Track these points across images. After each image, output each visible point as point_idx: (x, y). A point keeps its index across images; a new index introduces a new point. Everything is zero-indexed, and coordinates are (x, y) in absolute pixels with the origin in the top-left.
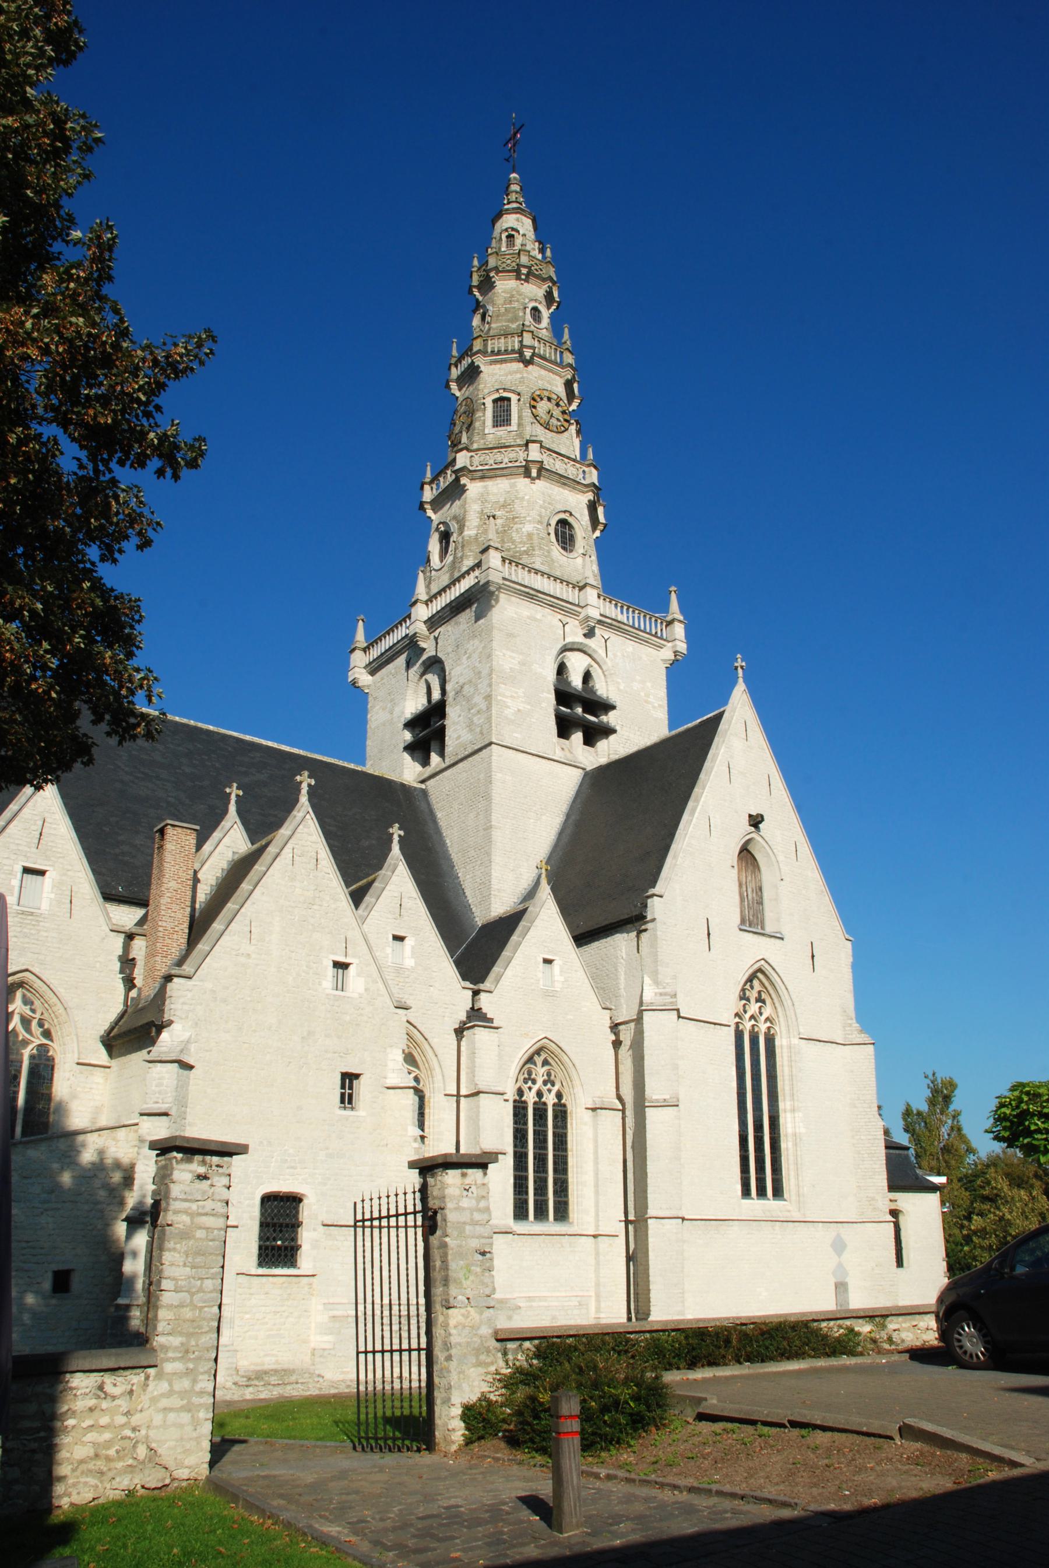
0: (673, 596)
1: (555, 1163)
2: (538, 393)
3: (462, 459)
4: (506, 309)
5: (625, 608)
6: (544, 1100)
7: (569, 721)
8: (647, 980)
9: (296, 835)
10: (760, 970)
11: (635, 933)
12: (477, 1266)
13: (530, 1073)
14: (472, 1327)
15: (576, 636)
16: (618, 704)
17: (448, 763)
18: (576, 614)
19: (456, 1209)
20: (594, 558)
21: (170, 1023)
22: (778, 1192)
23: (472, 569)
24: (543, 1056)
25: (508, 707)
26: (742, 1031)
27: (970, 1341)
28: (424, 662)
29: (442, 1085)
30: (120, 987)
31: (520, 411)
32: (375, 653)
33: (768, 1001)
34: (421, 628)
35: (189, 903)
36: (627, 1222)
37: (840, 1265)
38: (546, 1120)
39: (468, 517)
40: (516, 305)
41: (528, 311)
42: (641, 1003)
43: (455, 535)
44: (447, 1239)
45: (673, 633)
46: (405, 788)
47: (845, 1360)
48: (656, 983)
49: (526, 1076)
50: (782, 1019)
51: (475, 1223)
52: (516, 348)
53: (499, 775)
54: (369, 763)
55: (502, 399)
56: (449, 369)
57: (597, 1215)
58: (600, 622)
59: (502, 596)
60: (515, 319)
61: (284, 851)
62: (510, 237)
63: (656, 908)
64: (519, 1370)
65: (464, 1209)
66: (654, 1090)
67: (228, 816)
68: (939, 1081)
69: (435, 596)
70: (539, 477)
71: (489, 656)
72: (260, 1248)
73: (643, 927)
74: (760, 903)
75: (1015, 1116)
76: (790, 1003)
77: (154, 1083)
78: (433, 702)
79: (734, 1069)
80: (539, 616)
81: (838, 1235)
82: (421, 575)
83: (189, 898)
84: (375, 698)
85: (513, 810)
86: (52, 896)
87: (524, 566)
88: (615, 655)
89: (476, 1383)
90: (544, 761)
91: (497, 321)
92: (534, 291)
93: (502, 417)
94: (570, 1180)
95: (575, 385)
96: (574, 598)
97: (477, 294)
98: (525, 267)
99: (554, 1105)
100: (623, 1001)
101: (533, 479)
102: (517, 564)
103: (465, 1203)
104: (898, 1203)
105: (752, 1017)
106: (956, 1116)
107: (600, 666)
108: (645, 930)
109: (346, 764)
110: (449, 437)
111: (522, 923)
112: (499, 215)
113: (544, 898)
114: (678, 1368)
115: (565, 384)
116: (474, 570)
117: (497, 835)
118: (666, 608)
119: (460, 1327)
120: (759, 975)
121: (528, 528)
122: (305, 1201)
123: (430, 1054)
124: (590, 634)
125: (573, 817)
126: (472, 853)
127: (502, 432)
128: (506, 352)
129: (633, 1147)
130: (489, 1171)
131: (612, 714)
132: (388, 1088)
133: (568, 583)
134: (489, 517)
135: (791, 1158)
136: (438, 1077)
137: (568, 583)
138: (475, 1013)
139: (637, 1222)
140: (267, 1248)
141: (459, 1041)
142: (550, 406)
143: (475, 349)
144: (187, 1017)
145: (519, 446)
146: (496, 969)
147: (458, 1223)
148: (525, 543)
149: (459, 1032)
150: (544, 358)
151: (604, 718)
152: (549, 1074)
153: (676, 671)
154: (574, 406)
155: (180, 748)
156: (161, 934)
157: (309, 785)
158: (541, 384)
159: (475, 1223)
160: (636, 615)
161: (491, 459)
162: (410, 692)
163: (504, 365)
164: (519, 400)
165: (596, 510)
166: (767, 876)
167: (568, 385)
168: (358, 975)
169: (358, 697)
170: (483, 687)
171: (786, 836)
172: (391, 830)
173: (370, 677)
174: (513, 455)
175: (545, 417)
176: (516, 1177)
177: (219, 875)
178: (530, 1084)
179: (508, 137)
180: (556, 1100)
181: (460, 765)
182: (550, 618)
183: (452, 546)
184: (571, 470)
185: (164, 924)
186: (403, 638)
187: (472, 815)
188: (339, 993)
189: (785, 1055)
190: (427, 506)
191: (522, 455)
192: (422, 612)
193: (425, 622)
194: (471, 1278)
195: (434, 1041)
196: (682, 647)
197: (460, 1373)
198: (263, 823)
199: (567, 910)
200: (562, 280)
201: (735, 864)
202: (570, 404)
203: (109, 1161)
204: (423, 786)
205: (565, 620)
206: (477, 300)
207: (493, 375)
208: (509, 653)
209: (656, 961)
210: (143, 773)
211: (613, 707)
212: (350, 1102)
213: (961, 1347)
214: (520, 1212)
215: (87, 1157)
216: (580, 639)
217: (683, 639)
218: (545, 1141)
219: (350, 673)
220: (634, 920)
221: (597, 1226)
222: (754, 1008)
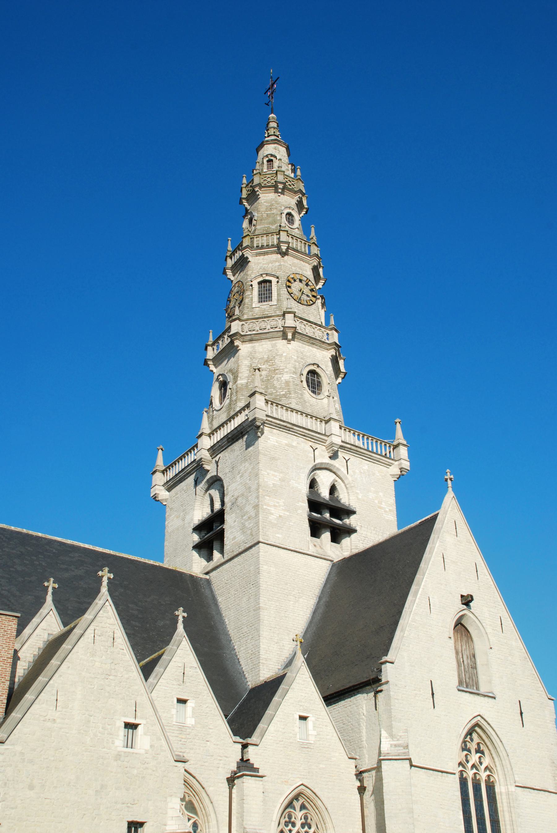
3: (235, 327)
4: (267, 215)
5: (361, 436)
7: (320, 524)
8: (384, 733)
9: (97, 619)
10: (477, 725)
11: (373, 694)
13: (290, 817)
15: (323, 457)
16: (357, 510)
17: (227, 557)
18: (324, 441)
23: (243, 409)
24: (301, 801)
26: (466, 779)
28: (208, 480)
29: (216, 829)
31: (278, 290)
32: (171, 474)
33: (486, 752)
34: (205, 454)
35: (8, 678)
39: (241, 370)
40: (274, 211)
42: (380, 753)
43: (231, 384)
45: (398, 454)
48: (391, 736)
50: (499, 768)
52: (275, 243)
53: (265, 567)
54: (166, 560)
55: (265, 281)
56: (226, 260)
58: (341, 447)
59: (266, 428)
60: (274, 222)
61: (87, 632)
62: (270, 161)
63: (389, 672)
69: (216, 430)
70: (293, 339)
71: (257, 475)
73: (379, 689)
74: (475, 667)
76: (505, 755)
78: (215, 511)
80: (294, 444)
82: (205, 414)
83: (8, 674)
85: (277, 595)
87: (282, 406)
88: (354, 472)
92: (289, 201)
95: (321, 270)
100: (365, 751)
102: (277, 405)
105: (474, 766)
108: (381, 691)
109: (147, 561)
111: (282, 686)
112: (262, 145)
113: (299, 665)
117: (264, 615)
118: (393, 435)
120: (477, 729)
121: (286, 377)
124: (334, 456)
125: (324, 600)
126: (245, 629)
127: (265, 306)
131: (353, 517)
133: (317, 418)
134: (255, 369)
136: (213, 822)
137: (317, 418)
138: (245, 764)
141: (231, 788)
143: (244, 245)
145: (278, 316)
146: (261, 726)
148: (283, 389)
149: (231, 781)
150: (297, 251)
151: (347, 521)
152: (306, 818)
153: (401, 480)
154: (320, 285)
155: (14, 551)
158: (294, 269)
160: (370, 441)
161: (257, 326)
162: (197, 504)
163: (266, 257)
164: (278, 282)
165: (337, 362)
166: (479, 645)
167: (315, 269)
168: (145, 734)
171: (491, 612)
172: (177, 613)
173: (167, 493)
174: (273, 323)
177: (36, 653)
179: (268, 87)
181: (236, 560)
182: (305, 445)
183: (229, 392)
184: (318, 333)
186: (192, 462)
187: (245, 599)
188: (129, 750)
189: (505, 801)
190: (210, 363)
191: (280, 323)
192: (206, 443)
193: (208, 450)
195: (210, 790)
196: (406, 465)
198: (73, 610)
199: (318, 675)
200: (310, 192)
204: (207, 577)
206: (246, 208)
207: (258, 264)
208: (272, 472)
209: (390, 717)
211: (354, 512)
216: (327, 460)
219: (152, 490)
220: (372, 683)
222: (474, 758)
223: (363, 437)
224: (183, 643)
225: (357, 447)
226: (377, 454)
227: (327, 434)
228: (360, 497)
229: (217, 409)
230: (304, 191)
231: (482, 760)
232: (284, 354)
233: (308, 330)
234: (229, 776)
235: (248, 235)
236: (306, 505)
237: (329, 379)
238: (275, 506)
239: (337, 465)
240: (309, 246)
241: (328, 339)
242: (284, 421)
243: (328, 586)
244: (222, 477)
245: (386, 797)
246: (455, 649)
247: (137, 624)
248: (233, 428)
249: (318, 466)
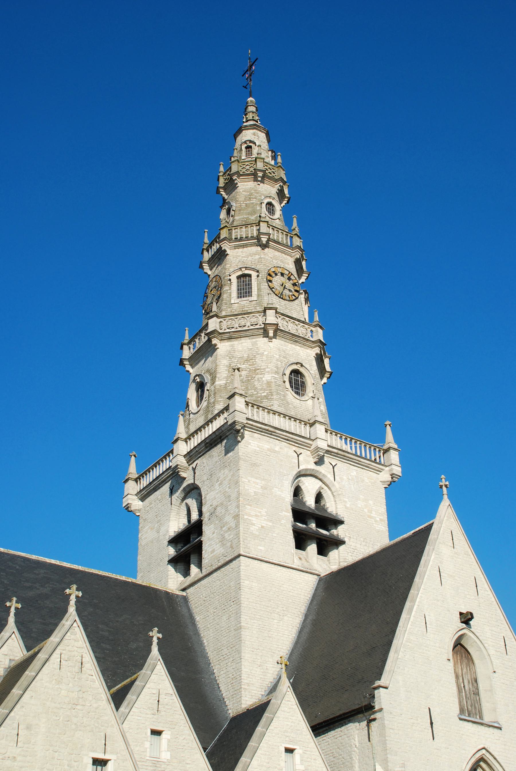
2: (273, 270)
4: (246, 205)
10: (482, 759)
11: (365, 723)
15: (308, 462)
16: (345, 519)
17: (205, 572)
18: (309, 446)
20: (322, 400)
23: (222, 412)
25: (254, 524)
31: (259, 285)
32: (145, 482)
34: (181, 461)
40: (254, 201)
41: (264, 205)
43: (208, 385)
45: (389, 459)
52: (255, 235)
53: (247, 582)
54: (139, 575)
55: (244, 276)
56: (202, 253)
58: (327, 452)
59: (246, 433)
60: (254, 212)
61: (52, 657)
62: (249, 148)
63: (382, 698)
69: (192, 435)
70: (275, 336)
71: (237, 483)
73: (372, 717)
80: (277, 449)
82: (181, 418)
84: (145, 520)
85: (259, 614)
87: (264, 408)
88: (341, 479)
92: (269, 190)
93: (245, 290)
95: (304, 263)
96: (306, 433)
97: (223, 193)
101: (271, 338)
102: (259, 407)
107: (329, 488)
108: (374, 720)
109: (118, 577)
110: (203, 307)
111: (266, 715)
112: (240, 131)
113: (285, 690)
115: (295, 262)
116: (223, 413)
117: (246, 635)
118: (383, 439)
120: (482, 764)
121: (267, 377)
124: (320, 462)
125: (310, 618)
126: (225, 651)
127: (244, 302)
131: (341, 528)
134: (235, 369)
137: (301, 421)
142: (284, 280)
143: (222, 237)
145: (258, 312)
148: (265, 390)
151: (334, 532)
153: (392, 487)
154: (303, 279)
157: (77, 597)
158: (275, 263)
160: (358, 445)
161: (236, 323)
162: (173, 514)
163: (245, 249)
164: (258, 276)
165: (322, 361)
166: (481, 669)
167: (298, 263)
170: (232, 509)
172: (151, 634)
173: (141, 503)
174: (254, 320)
175: (280, 289)
179: (245, 70)
181: (215, 574)
182: (287, 450)
184: (301, 330)
187: (225, 618)
190: (186, 362)
191: (260, 320)
192: (182, 448)
193: (185, 456)
196: (398, 470)
198: (37, 632)
199: (305, 702)
200: (291, 180)
201: (451, 657)
202: (300, 278)
204: (184, 594)
205: (299, 451)
206: (224, 198)
207: (237, 257)
208: (253, 480)
211: (342, 522)
216: (312, 466)
217: (398, 464)
219: (124, 500)
223: (351, 441)
224: (157, 667)
225: (344, 451)
226: (365, 458)
228: (348, 506)
230: (285, 180)
232: (265, 353)
235: (226, 226)
236: (290, 515)
237: (314, 379)
238: (256, 516)
239: (323, 472)
240: (291, 238)
241: (312, 336)
242: (266, 425)
244: (200, 485)
246: (455, 672)
248: (211, 433)
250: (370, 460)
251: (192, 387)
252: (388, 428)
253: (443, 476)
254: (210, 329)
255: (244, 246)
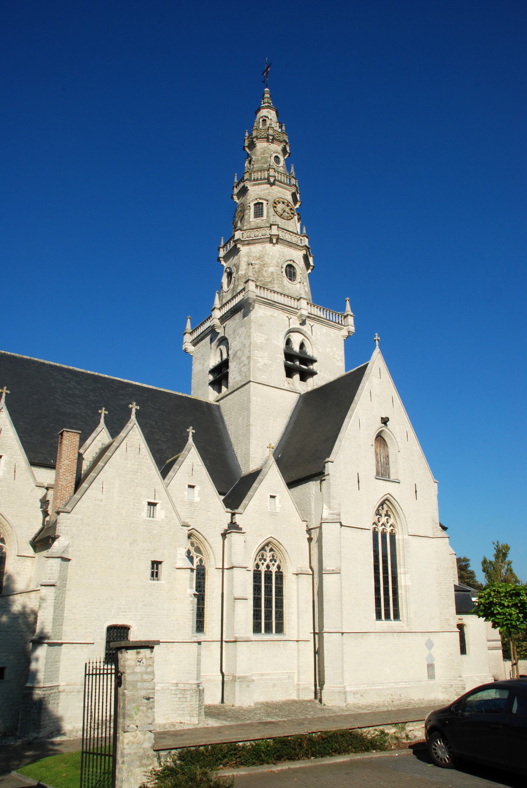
0: (348, 302)
1: (276, 603)
2: (277, 200)
5: (322, 309)
6: (270, 569)
7: (292, 369)
8: (325, 506)
9: (128, 436)
10: (387, 499)
11: (319, 481)
12: (144, 706)
13: (263, 556)
14: (139, 743)
15: (295, 323)
16: (318, 359)
18: (296, 313)
19: (132, 673)
21: (59, 536)
22: (397, 616)
23: (241, 291)
24: (270, 546)
25: (259, 362)
26: (377, 532)
27: (441, 750)
28: (219, 339)
29: (214, 563)
30: (41, 515)
31: (268, 209)
32: (196, 335)
33: (392, 516)
34: (217, 322)
36: (315, 633)
37: (430, 655)
38: (272, 580)
40: (266, 155)
41: (273, 158)
43: (234, 274)
44: (126, 691)
45: (347, 322)
46: (208, 405)
47: (375, 754)
48: (330, 508)
49: (261, 557)
50: (399, 525)
51: (143, 681)
52: (266, 177)
53: (254, 398)
55: (259, 203)
56: (233, 189)
57: (298, 630)
58: (308, 317)
59: (256, 305)
60: (266, 162)
62: (264, 121)
63: (330, 468)
64: (167, 768)
65: (137, 673)
66: (327, 565)
67: (100, 425)
68: (500, 546)
70: (277, 243)
71: (249, 336)
72: (106, 654)
73: (323, 478)
74: (388, 464)
75: (487, 604)
77: (49, 568)
79: (372, 552)
80: (276, 315)
81: (429, 639)
82: (217, 295)
84: (196, 358)
85: (262, 415)
86: (5, 469)
87: (268, 289)
89: (139, 777)
90: (278, 390)
91: (257, 164)
92: (277, 148)
93: (259, 213)
94: (284, 612)
97: (247, 150)
98: (271, 135)
99: (276, 572)
100: (313, 517)
101: (274, 244)
102: (264, 288)
103: (138, 669)
104: (463, 620)
105: (383, 524)
106: (509, 563)
108: (324, 480)
109: (177, 393)
110: (233, 223)
111: (259, 477)
112: (259, 110)
113: (271, 464)
114: (268, 763)
115: (292, 195)
116: (242, 292)
117: (253, 429)
118: (344, 309)
119: (131, 744)
120: (387, 502)
121: (271, 269)
122: (131, 629)
123: (208, 547)
124: (303, 323)
125: (293, 419)
126: (241, 438)
127: (258, 220)
128: (261, 179)
129: (318, 594)
130: (155, 650)
132: (177, 569)
135: (404, 598)
136: (212, 559)
137: (291, 297)
138: (233, 525)
139: (318, 634)
140: (110, 654)
142: (284, 206)
143: (245, 178)
144: (67, 533)
145: (267, 227)
146: (244, 502)
147: (133, 681)
148: (269, 277)
150: (281, 182)
151: (311, 367)
152: (273, 556)
153: (349, 341)
154: (297, 206)
155: (89, 387)
156: (60, 488)
157: (136, 409)
158: (279, 195)
159: (143, 681)
160: (328, 313)
161: (252, 234)
163: (260, 186)
164: (267, 204)
166: (392, 450)
167: (294, 195)
168: (162, 509)
169: (188, 357)
170: (246, 352)
171: (401, 428)
172: (188, 430)
173: (193, 347)
174: (264, 232)
175: (281, 212)
176: (254, 611)
178: (263, 561)
179: (264, 70)
180: (277, 570)
181: (235, 393)
182: (282, 316)
183: (233, 279)
184: (294, 239)
185: (62, 483)
186: (209, 327)
187: (241, 419)
188: (151, 519)
189: (401, 544)
190: (221, 259)
192: (217, 314)
193: (219, 319)
194: (139, 714)
195: (210, 540)
196: (352, 329)
197: (129, 772)
198: (116, 428)
201: (374, 444)
202: (295, 205)
203: (28, 610)
204: (218, 404)
205: (290, 316)
207: (254, 191)
208: (259, 334)
209: (329, 496)
210: (68, 400)
212: (157, 576)
213: (436, 753)
214: (257, 629)
215: (16, 608)
216: (298, 326)
218: (271, 591)
219: (183, 345)
220: (319, 475)
221: (298, 636)
222: (384, 519)
223: (323, 310)
224: (192, 450)
225: (318, 317)
226: (332, 321)
227: (298, 308)
228: (320, 351)
229: (226, 291)
230: (287, 141)
231: (389, 521)
232: (271, 254)
233: (288, 237)
234: (223, 532)
235: (248, 171)
236: (283, 356)
237: (301, 270)
238: (261, 357)
239: (305, 329)
240: (290, 179)
241: (301, 243)
242: (269, 300)
243: (296, 410)
244: (228, 338)
245: (324, 544)
246: (375, 451)
247: (170, 434)
248: (234, 304)
249: (292, 330)
250: (335, 322)
251: (225, 275)
252: (348, 302)
253: (376, 334)
254: (236, 238)
255: (260, 184)
